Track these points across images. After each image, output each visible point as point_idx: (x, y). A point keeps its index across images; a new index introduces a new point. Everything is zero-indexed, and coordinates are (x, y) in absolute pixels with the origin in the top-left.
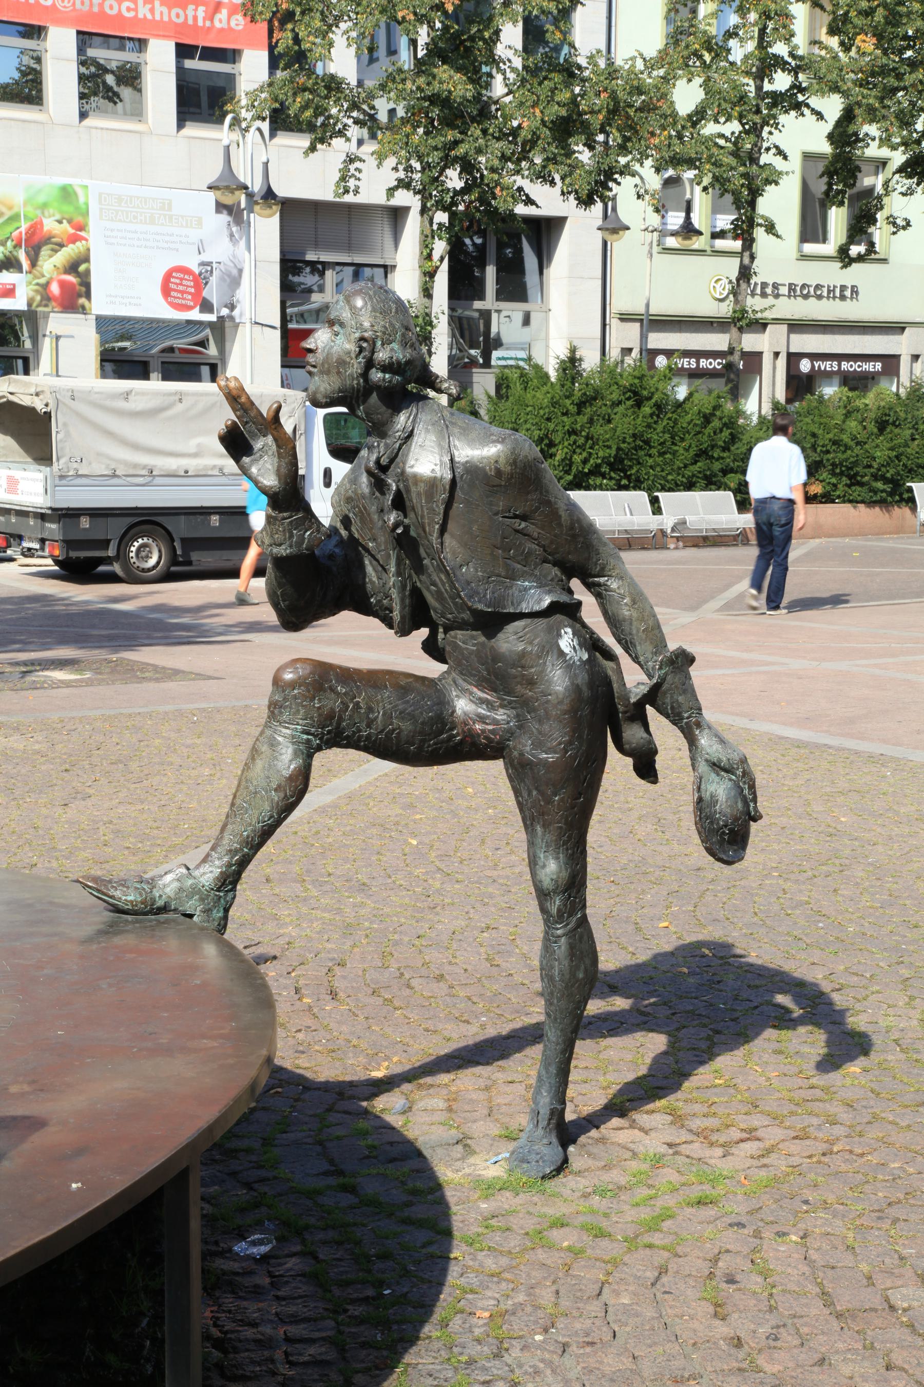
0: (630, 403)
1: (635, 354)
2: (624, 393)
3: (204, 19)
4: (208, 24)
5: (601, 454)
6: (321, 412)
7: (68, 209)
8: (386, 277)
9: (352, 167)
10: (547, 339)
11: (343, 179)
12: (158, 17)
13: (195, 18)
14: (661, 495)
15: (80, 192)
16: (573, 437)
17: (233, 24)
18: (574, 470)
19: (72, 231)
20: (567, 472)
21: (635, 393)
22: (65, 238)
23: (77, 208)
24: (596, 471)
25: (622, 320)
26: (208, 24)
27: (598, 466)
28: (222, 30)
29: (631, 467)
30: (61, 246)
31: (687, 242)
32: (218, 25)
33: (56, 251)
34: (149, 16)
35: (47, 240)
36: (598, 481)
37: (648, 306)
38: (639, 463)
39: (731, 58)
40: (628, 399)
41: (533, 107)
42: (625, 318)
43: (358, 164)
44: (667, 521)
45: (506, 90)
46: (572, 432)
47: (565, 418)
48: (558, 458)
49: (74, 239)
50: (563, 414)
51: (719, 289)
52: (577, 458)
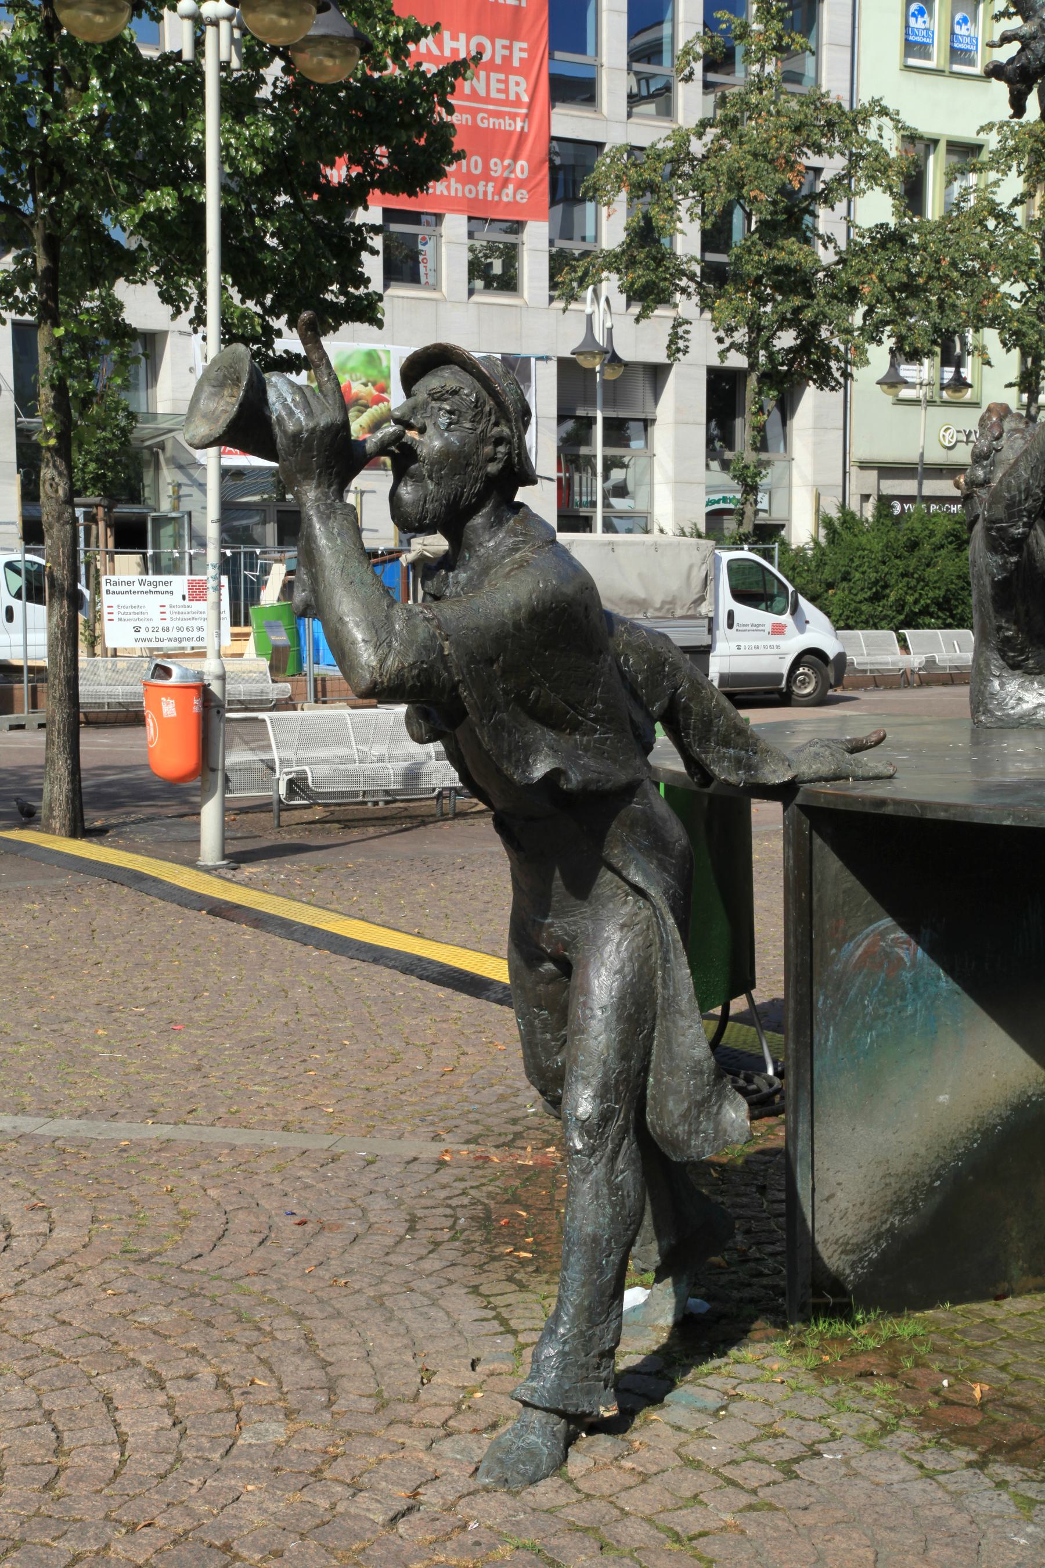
0: (953, 546)
1: (872, 500)
2: (947, 537)
3: (493, 194)
4: (496, 198)
5: (931, 594)
6: (727, 556)
7: (373, 373)
8: (646, 429)
9: (680, 331)
10: (652, 484)
11: (671, 342)
12: (453, 194)
13: (485, 193)
14: (906, 632)
15: (382, 355)
16: (906, 579)
17: (518, 197)
18: (907, 609)
19: (376, 393)
20: (899, 612)
21: (957, 537)
22: (370, 399)
23: (381, 372)
24: (925, 612)
25: (861, 468)
26: (496, 198)
27: (928, 606)
28: (509, 203)
29: (956, 607)
30: (367, 407)
31: (958, 394)
32: (505, 199)
33: (362, 412)
34: (445, 193)
35: (356, 401)
36: (927, 620)
37: (922, 455)
38: (964, 603)
39: (1016, 224)
40: (951, 543)
41: (869, 273)
42: (864, 466)
43: (686, 327)
44: (915, 660)
45: (837, 258)
46: (904, 575)
47: (897, 561)
48: (892, 598)
49: (378, 400)
50: (896, 557)
51: (948, 438)
52: (910, 599)
